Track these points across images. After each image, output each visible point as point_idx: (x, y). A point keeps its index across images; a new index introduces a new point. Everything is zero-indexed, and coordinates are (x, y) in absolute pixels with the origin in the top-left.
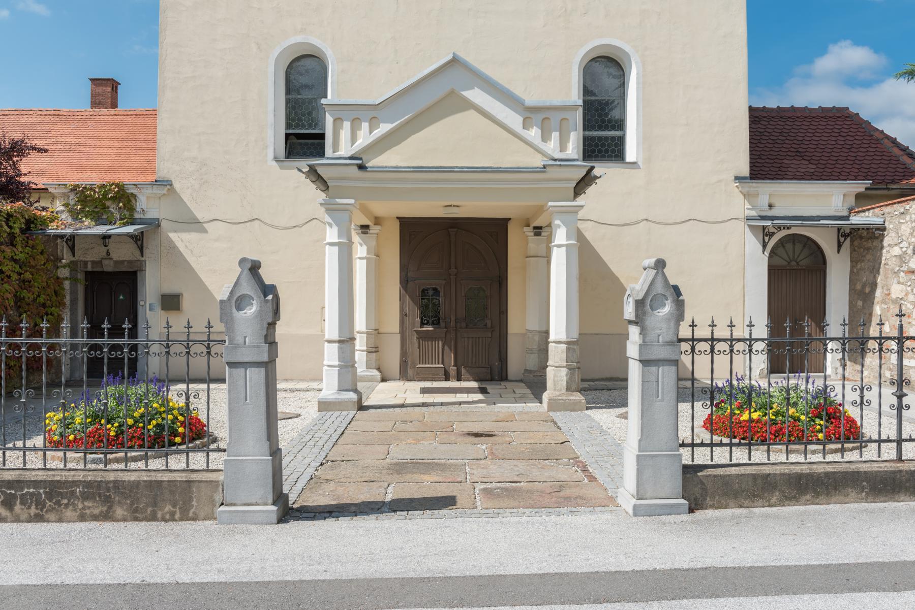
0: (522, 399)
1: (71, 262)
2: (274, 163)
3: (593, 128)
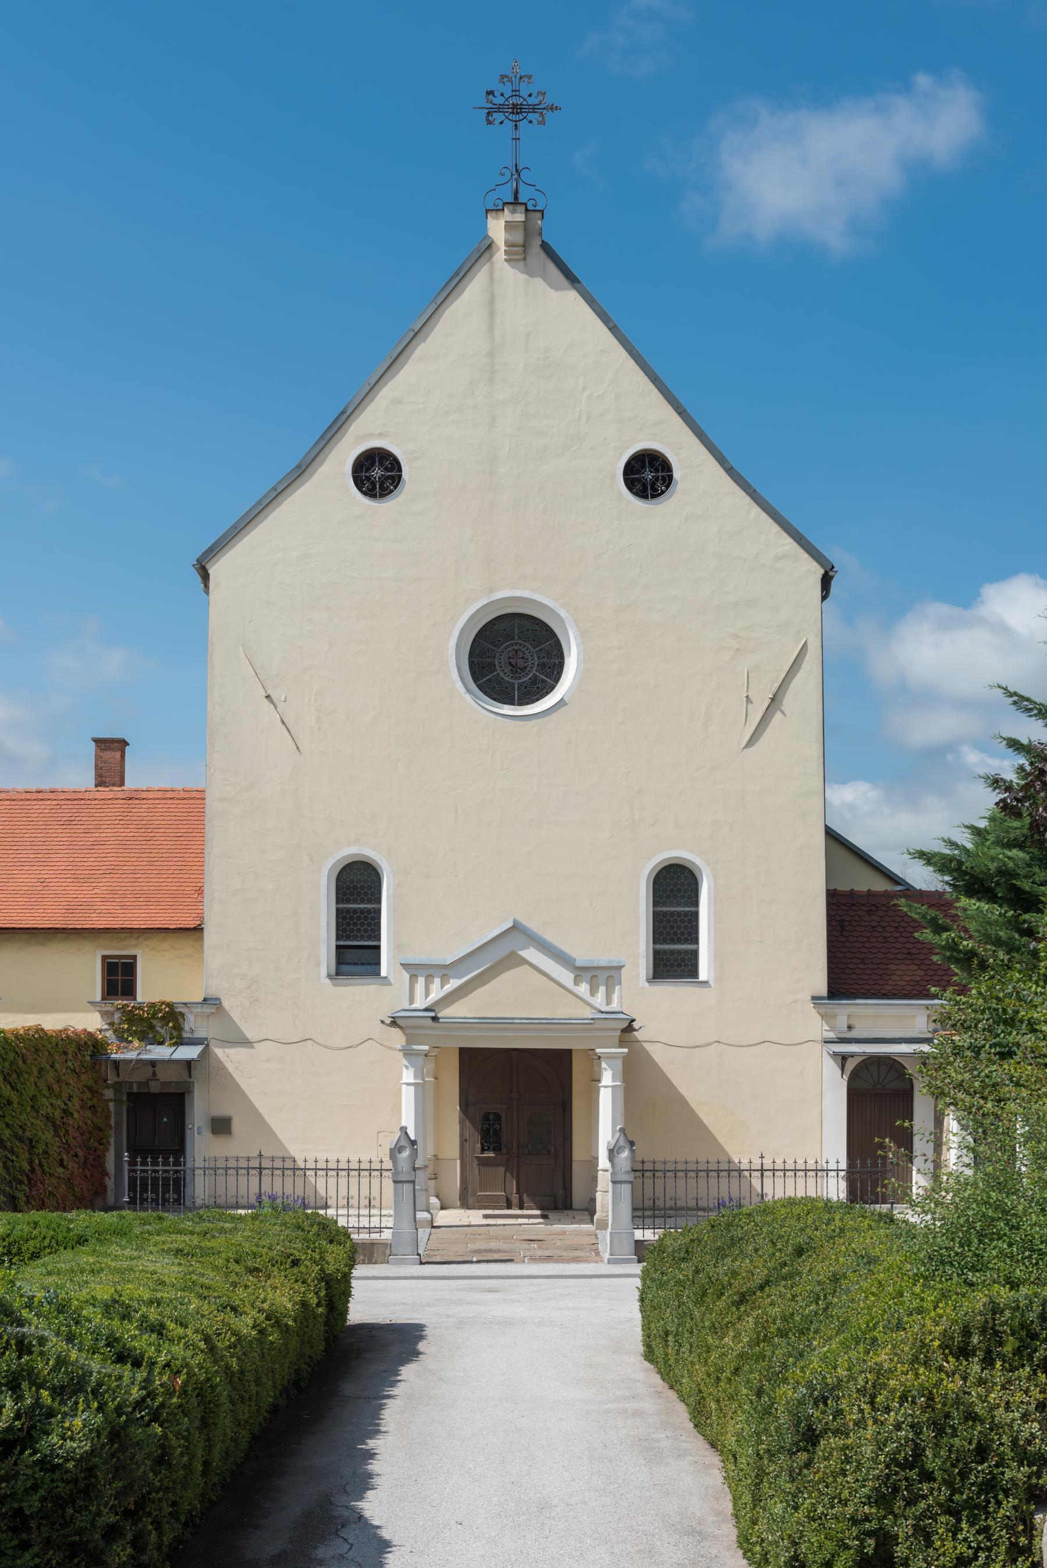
0: (580, 1222)
1: (116, 1083)
2: (328, 981)
3: (664, 941)
